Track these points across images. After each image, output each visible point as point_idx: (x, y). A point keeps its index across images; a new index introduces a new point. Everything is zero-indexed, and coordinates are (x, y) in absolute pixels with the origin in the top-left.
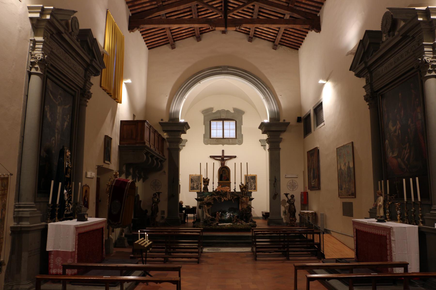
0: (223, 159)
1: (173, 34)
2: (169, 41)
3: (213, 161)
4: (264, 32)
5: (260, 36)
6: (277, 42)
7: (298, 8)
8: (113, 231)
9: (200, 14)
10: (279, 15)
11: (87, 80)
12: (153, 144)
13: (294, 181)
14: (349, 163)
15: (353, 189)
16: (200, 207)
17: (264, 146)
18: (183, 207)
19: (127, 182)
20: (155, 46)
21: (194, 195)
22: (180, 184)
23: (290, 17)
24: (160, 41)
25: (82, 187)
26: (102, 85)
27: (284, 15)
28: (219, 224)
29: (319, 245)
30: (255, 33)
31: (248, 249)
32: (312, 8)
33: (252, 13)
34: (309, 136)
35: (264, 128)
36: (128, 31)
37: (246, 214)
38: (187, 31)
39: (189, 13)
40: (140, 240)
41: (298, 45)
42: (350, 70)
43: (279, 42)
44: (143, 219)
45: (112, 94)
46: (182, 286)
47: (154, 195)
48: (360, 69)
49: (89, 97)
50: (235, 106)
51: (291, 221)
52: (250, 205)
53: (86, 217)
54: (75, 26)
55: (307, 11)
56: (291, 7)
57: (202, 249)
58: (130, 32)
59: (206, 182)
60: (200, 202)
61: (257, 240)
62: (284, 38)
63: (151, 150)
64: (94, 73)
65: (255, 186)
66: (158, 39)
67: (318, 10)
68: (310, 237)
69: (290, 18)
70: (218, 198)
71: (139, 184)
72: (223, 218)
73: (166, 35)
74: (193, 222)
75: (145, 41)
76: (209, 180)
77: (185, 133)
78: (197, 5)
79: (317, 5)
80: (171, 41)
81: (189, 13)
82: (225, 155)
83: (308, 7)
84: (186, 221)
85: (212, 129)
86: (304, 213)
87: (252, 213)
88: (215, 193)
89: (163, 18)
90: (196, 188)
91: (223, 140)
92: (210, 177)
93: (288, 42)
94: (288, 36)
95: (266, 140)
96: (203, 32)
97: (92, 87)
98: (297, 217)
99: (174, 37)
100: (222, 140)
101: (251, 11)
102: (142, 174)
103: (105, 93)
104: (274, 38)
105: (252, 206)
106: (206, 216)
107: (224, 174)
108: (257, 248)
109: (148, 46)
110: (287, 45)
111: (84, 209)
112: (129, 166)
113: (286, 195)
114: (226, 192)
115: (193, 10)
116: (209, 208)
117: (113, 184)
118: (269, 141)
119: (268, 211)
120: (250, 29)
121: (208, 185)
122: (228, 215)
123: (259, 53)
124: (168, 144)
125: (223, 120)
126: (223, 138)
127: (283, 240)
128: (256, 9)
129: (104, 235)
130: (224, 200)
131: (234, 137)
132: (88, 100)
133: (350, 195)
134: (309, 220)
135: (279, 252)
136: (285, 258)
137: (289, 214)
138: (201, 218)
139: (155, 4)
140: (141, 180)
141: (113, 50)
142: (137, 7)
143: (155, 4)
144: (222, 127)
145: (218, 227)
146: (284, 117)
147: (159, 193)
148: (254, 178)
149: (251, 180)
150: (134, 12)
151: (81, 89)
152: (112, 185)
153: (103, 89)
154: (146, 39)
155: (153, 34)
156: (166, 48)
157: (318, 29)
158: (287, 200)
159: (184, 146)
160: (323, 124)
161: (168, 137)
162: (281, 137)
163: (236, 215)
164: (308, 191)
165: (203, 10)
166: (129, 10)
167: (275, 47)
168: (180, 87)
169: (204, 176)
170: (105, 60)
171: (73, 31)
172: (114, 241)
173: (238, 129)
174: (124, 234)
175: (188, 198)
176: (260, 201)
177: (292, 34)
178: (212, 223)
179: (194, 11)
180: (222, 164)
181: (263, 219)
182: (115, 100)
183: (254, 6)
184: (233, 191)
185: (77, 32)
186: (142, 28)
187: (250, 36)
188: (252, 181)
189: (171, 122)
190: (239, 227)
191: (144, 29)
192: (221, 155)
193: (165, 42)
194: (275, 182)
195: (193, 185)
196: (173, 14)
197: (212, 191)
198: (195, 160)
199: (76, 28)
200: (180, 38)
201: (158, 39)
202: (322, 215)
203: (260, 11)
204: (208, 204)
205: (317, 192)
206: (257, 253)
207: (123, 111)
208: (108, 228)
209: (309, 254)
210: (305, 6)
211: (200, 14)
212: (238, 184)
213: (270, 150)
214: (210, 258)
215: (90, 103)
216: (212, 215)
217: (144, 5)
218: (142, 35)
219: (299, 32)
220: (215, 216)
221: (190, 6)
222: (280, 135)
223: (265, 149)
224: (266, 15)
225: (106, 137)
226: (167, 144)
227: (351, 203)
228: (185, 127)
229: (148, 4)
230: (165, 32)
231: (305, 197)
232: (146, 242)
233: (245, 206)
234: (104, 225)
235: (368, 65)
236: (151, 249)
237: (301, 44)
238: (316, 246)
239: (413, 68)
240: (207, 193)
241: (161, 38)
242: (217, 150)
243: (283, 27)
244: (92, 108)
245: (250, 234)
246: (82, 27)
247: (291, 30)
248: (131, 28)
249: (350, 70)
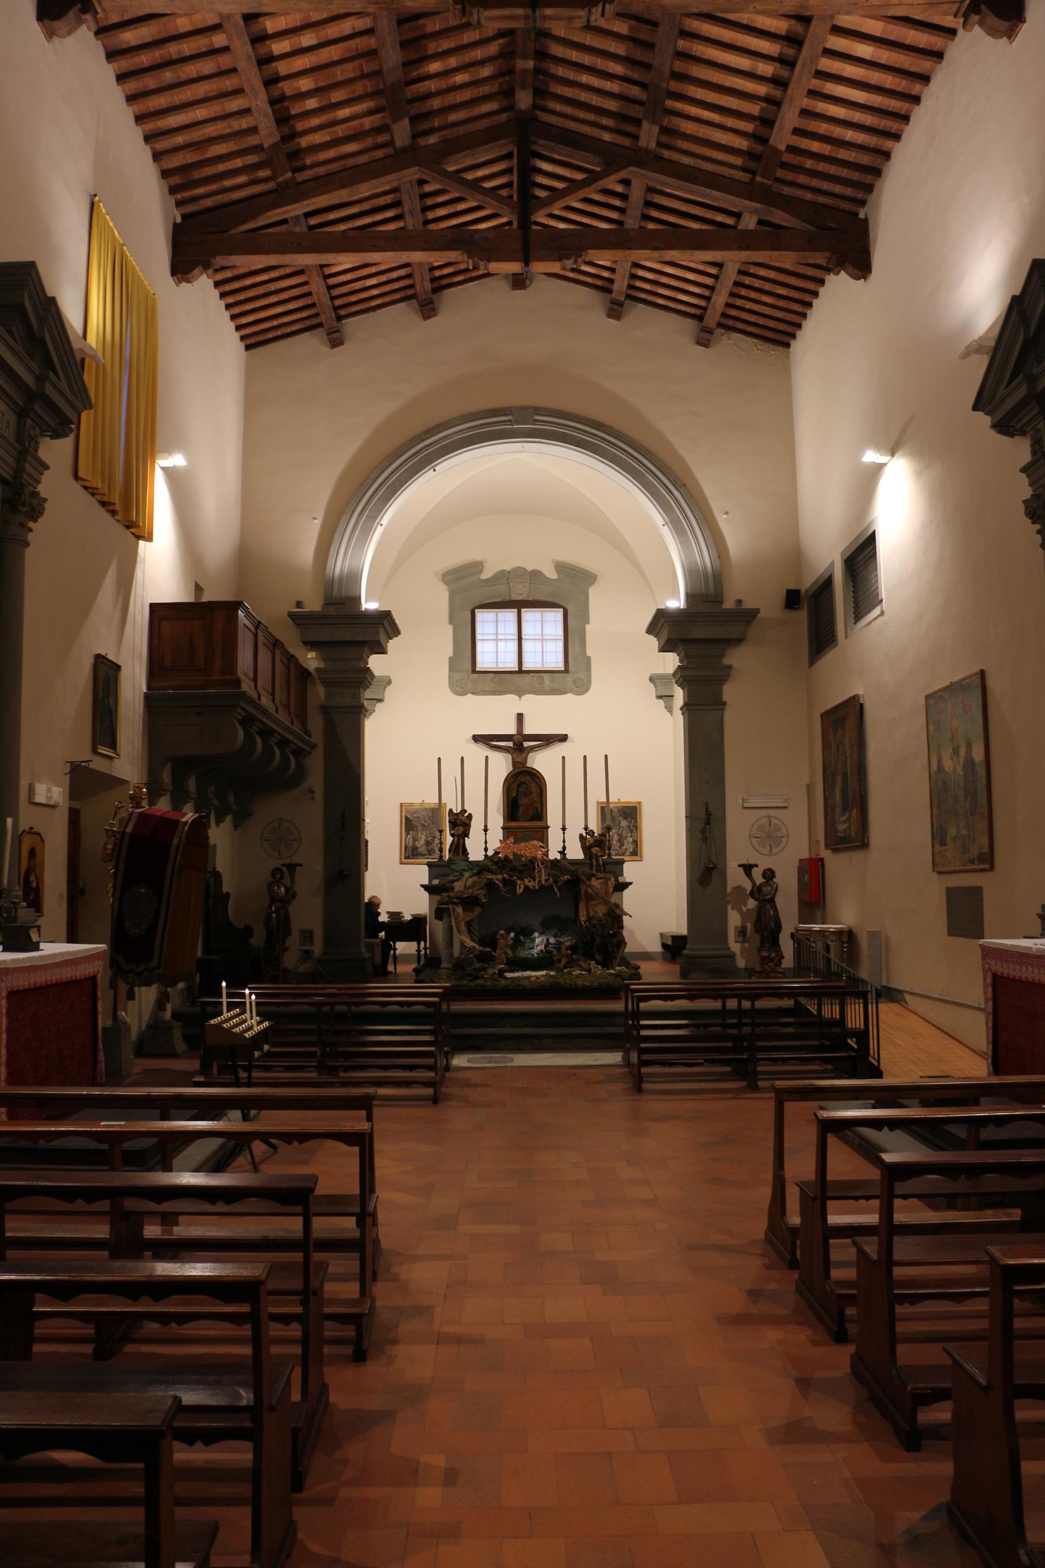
0: (519, 745)
1: (336, 292)
2: (322, 318)
3: (481, 751)
4: (664, 280)
5: (650, 298)
6: (712, 318)
7: (787, 190)
8: (131, 996)
9: (431, 215)
10: (720, 218)
11: (25, 451)
12: (265, 693)
13: (776, 818)
14: (969, 745)
15: (985, 840)
16: (440, 913)
17: (666, 698)
18: (381, 919)
19: (176, 822)
20: (270, 335)
21: (420, 873)
22: (367, 837)
23: (760, 222)
24: (286, 319)
25: (18, 839)
26: (82, 474)
27: (738, 216)
28: (509, 975)
29: (863, 1036)
30: (631, 287)
31: (615, 1058)
32: (838, 189)
33: (622, 210)
34: (829, 658)
35: (668, 629)
36: (170, 281)
37: (605, 937)
38: (383, 278)
39: (390, 214)
40: (226, 1015)
41: (789, 329)
42: (975, 408)
43: (717, 318)
44: (239, 955)
45: (118, 508)
46: (378, 1173)
47: (273, 874)
48: (1009, 405)
49: (35, 511)
50: (560, 558)
51: (765, 960)
52: (618, 906)
53: (35, 937)
55: (821, 199)
56: (762, 184)
57: (447, 1056)
58: (179, 282)
59: (461, 823)
60: (437, 898)
61: (642, 1022)
62: (739, 302)
63: (263, 710)
64: (52, 424)
65: (635, 842)
66: (279, 310)
67: (860, 195)
68: (830, 1011)
69: (759, 227)
70: (504, 881)
71: (220, 835)
72: (523, 953)
73: (309, 294)
74: (414, 970)
75: (233, 317)
76: (470, 816)
77: (383, 651)
78: (422, 182)
79: (855, 176)
80: (327, 316)
81: (390, 214)
82: (528, 730)
83: (825, 186)
84: (390, 968)
85: (478, 637)
86: (809, 930)
87: (625, 933)
88: (495, 863)
89: (298, 229)
90: (423, 849)
91: (518, 679)
92: (474, 807)
93: (752, 318)
94: (753, 295)
95: (674, 674)
96: (444, 282)
97: (47, 477)
98: (787, 945)
99: (338, 302)
100: (516, 677)
101: (617, 203)
102: (231, 798)
103: (93, 503)
104: (703, 303)
105: (626, 907)
106: (462, 944)
107: (524, 798)
108: (642, 1051)
109: (243, 338)
110: (750, 329)
111: (24, 914)
112: (183, 766)
113: (748, 869)
114: (532, 861)
115: (405, 199)
116: (471, 916)
117: (129, 830)
118: (683, 677)
119: (684, 931)
120: (612, 270)
121: (466, 834)
122: (539, 943)
123: (650, 362)
124: (321, 690)
125: (519, 605)
126: (520, 671)
127: (735, 1021)
128: (637, 194)
129: (100, 1004)
130: (526, 887)
131: (561, 666)
132: (31, 524)
133: (972, 862)
134: (828, 951)
135: (722, 1062)
136: (743, 1084)
137: (758, 937)
138: (444, 954)
139: (265, 180)
140: (229, 819)
141: (118, 346)
142: (200, 191)
143: (265, 180)
144: (516, 631)
145: (503, 982)
146: (739, 591)
147: (292, 868)
148: (631, 813)
149: (621, 823)
150: (191, 208)
152: (123, 833)
153: (86, 488)
154: (237, 310)
155: (260, 290)
156: (311, 343)
157: (860, 264)
158: (748, 886)
159: (380, 700)
160: (877, 611)
161: (322, 665)
162: (726, 661)
163: (567, 941)
164: (826, 854)
165: (441, 199)
166: (172, 201)
167: (704, 338)
168: (363, 486)
169: (452, 803)
170: (89, 378)
172: (134, 1036)
173: (572, 637)
174: (169, 1006)
175: (396, 885)
176: (655, 898)
177: (767, 286)
178: (484, 969)
179: (411, 203)
180: (515, 763)
181: (665, 959)
182: (128, 527)
183: (626, 182)
184: (559, 857)
186: (223, 268)
187: (614, 295)
188: (624, 823)
189: (331, 610)
190: (580, 982)
191: (228, 274)
192: (512, 730)
193: (308, 323)
194: (708, 822)
195: (415, 840)
196: (332, 216)
197: (480, 857)
198: (420, 750)
200: (362, 307)
201: (279, 310)
202: (874, 936)
203: (649, 204)
204: (469, 902)
205: (857, 856)
206: (644, 1070)
207: (160, 570)
208: (113, 985)
209: (826, 1071)
210: (814, 183)
211: (431, 215)
212: (575, 830)
213: (688, 708)
214: (476, 1085)
215: (40, 532)
216: (482, 942)
217: (228, 183)
218: (223, 295)
219: (793, 281)
220: (494, 945)
221: (395, 184)
222: (722, 656)
223: (669, 709)
224: (672, 219)
225: (100, 660)
226: (319, 693)
228: (380, 629)
229: (242, 179)
230: (306, 283)
231: (813, 880)
232: (252, 1024)
233: (601, 910)
234: (100, 969)
235: (1040, 388)
236: (266, 1047)
237: (799, 326)
238: (852, 1042)
240: (463, 865)
241: (291, 306)
242: (498, 714)
243: (733, 259)
244: (47, 550)
245: (618, 1006)
247: (762, 272)
248: (182, 268)
249: (975, 408)
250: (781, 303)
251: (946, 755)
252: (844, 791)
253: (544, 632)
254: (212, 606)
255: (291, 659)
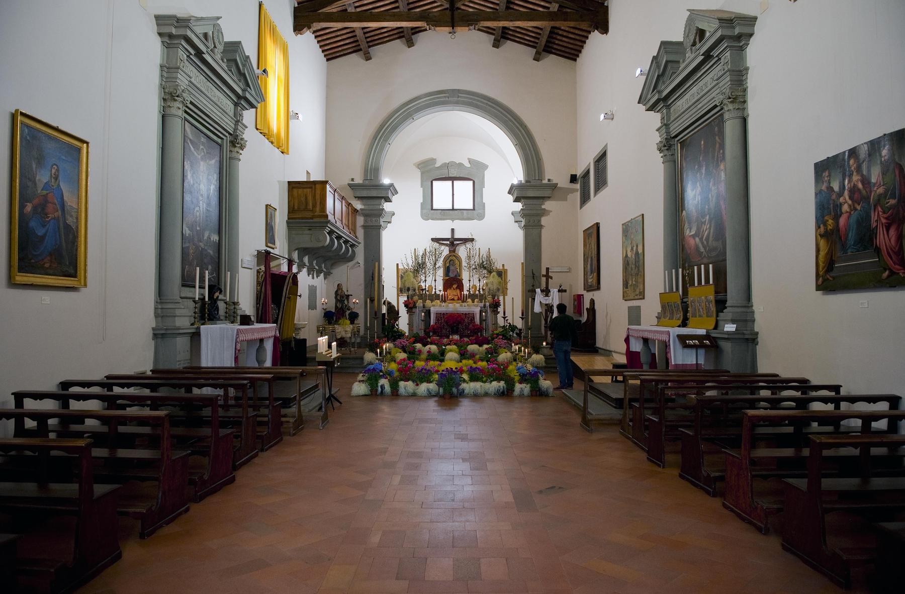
0: (453, 243)
11: (238, 121)
34: (588, 205)
54: (218, 36)
66: (342, 43)
75: (321, 47)
82: (456, 236)
91: (452, 213)
99: (369, 40)
125: (453, 179)
126: (453, 209)
151: (230, 134)
154: (322, 43)
156: (355, 58)
159: (389, 222)
164: (584, 293)
171: (215, 47)
173: (477, 193)
185: (220, 48)
192: (449, 236)
199: (219, 42)
201: (342, 43)
219: (577, 32)
226: (360, 220)
227: (639, 307)
239: (716, 106)
241: (347, 41)
246: (228, 38)
248: (298, 28)
250: (572, 41)
251: (629, 249)
252: (591, 265)
253: (464, 190)
254: (315, 183)
255: (349, 204)
